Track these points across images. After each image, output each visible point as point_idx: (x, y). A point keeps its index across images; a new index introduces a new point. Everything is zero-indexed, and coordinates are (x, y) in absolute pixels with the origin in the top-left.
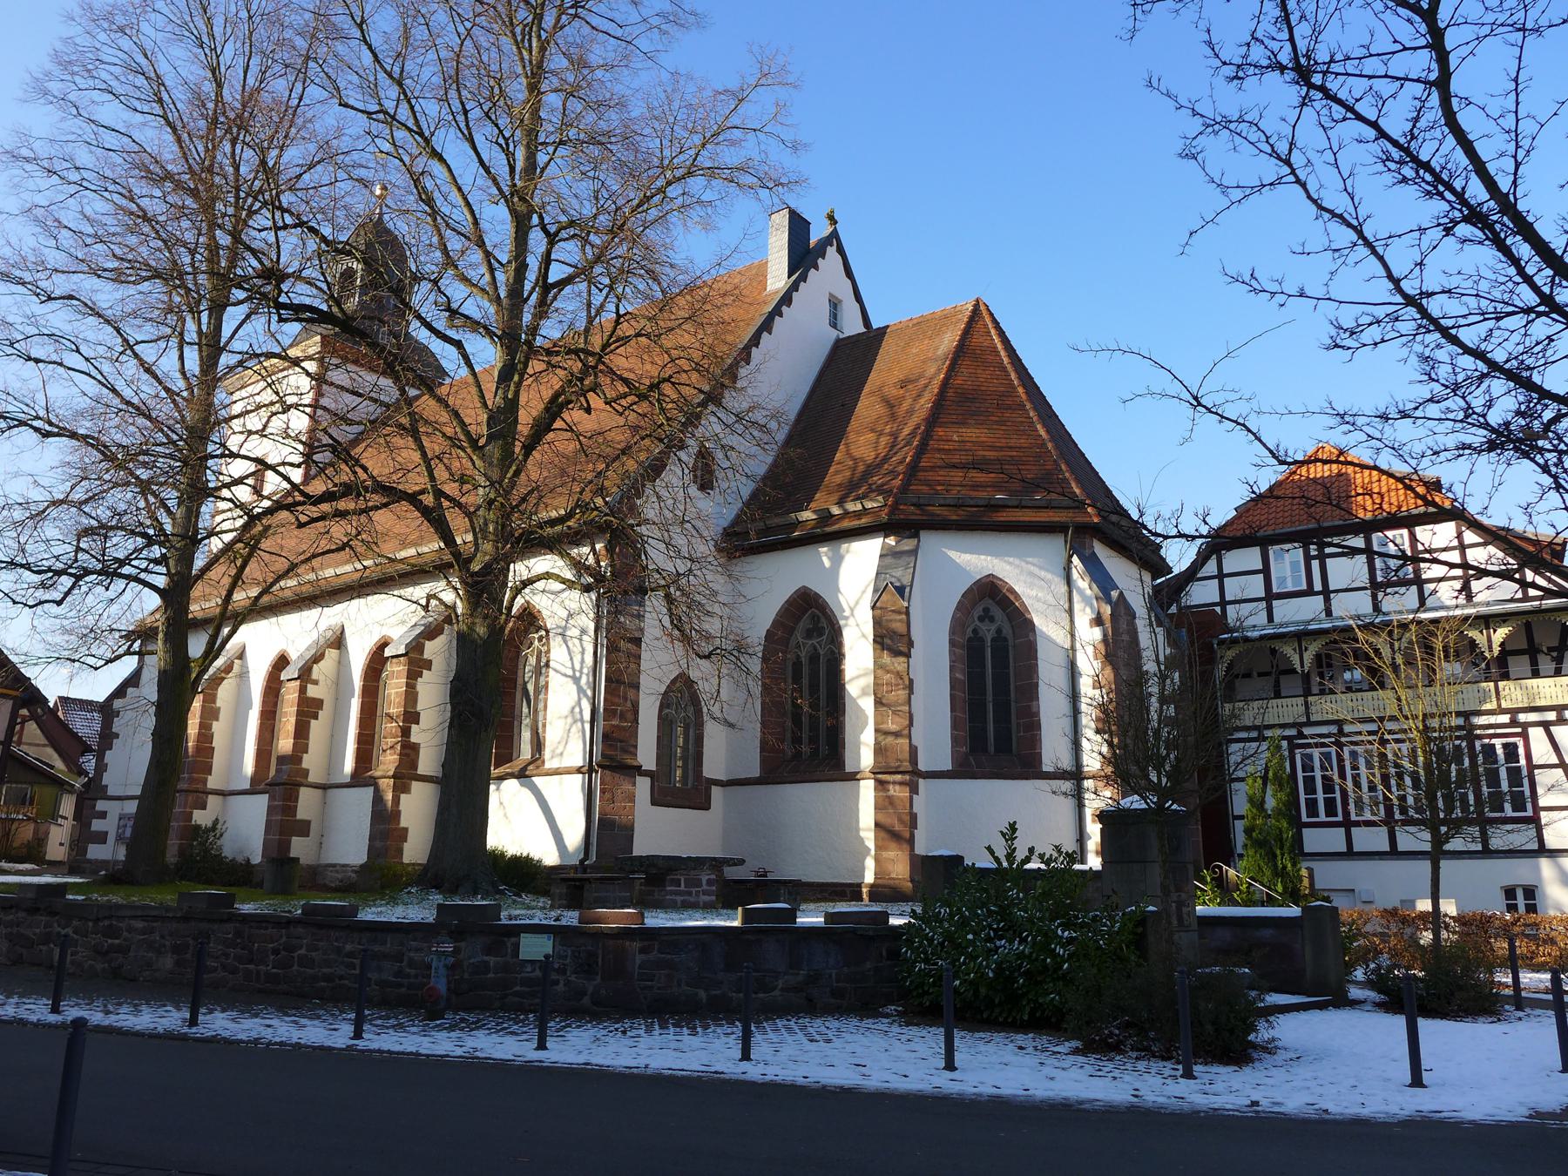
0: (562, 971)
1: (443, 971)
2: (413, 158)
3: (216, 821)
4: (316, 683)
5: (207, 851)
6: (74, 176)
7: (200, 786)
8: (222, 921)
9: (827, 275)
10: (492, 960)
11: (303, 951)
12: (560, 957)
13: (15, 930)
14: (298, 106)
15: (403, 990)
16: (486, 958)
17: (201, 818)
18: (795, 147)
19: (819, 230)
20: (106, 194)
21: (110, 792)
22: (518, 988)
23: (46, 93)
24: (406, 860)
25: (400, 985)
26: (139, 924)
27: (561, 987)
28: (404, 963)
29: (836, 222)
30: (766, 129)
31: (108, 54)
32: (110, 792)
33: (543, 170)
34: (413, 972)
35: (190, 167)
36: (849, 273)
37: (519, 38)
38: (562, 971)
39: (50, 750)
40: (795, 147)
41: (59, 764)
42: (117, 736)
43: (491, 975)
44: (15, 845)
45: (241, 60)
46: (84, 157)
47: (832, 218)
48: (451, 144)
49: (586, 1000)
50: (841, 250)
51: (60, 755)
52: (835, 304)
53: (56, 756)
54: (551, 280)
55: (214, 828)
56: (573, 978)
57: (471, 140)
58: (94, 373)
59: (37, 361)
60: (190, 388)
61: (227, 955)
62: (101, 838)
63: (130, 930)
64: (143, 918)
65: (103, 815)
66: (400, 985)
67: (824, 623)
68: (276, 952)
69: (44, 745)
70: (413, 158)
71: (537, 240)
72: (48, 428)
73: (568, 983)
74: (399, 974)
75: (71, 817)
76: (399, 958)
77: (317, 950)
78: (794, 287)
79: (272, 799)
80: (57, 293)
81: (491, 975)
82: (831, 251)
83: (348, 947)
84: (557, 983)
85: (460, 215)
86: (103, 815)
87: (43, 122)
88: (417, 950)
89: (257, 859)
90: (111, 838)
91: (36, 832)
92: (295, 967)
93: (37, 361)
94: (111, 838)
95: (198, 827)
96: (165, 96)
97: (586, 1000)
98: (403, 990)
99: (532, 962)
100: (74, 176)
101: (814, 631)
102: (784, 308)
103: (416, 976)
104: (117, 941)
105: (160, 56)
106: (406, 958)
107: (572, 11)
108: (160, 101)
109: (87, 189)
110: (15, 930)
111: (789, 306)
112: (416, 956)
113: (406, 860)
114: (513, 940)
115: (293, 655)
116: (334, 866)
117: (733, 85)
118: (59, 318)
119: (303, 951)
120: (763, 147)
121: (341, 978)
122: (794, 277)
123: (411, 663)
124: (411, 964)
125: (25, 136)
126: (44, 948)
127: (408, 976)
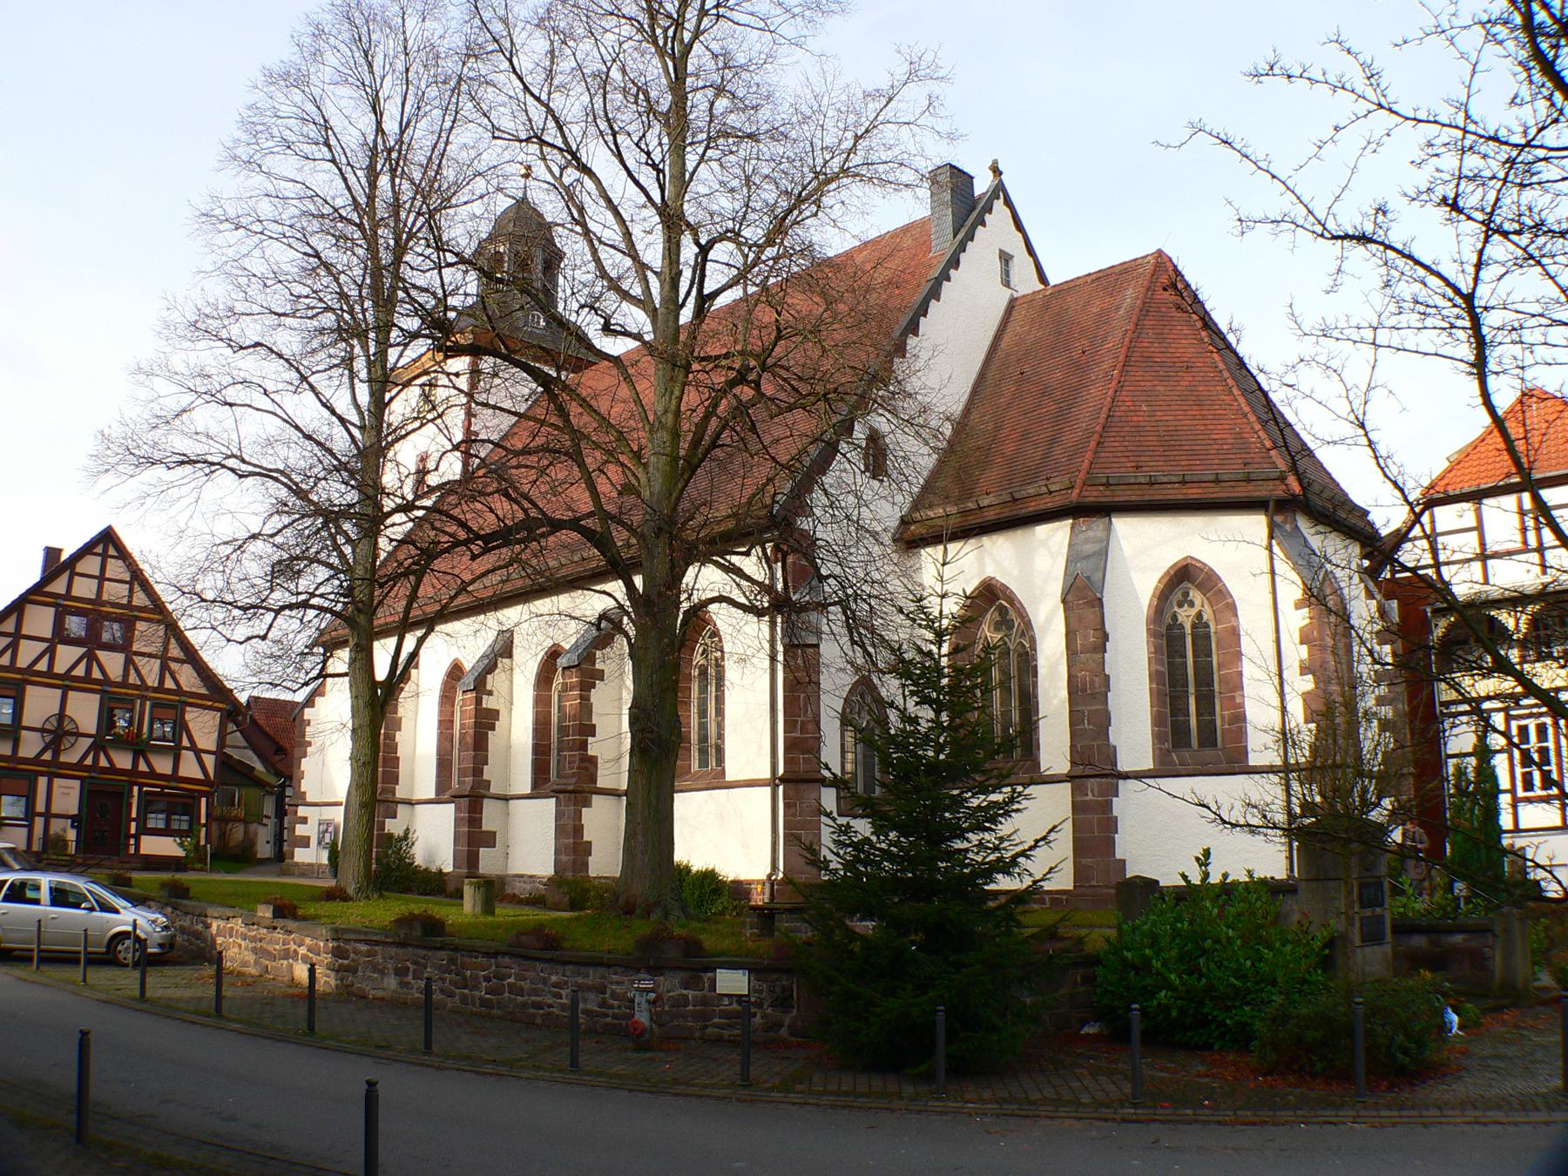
0: (760, 1005)
1: (644, 1005)
2: (562, 169)
3: (407, 831)
4: (490, 693)
5: (402, 859)
6: (257, 227)
7: (389, 796)
8: (436, 949)
9: (996, 231)
10: (690, 994)
11: (512, 980)
12: (756, 991)
13: (259, 945)
14: (452, 127)
15: (609, 1020)
16: (684, 992)
17: (394, 827)
18: (951, 137)
19: (982, 184)
20: (285, 240)
21: (309, 799)
22: (717, 1020)
23: (235, 158)
24: (592, 873)
25: (607, 1015)
26: (364, 948)
27: (757, 1020)
28: (607, 995)
29: (1001, 173)
30: (919, 122)
31: (285, 109)
32: (309, 799)
33: (692, 174)
34: (616, 1003)
35: (354, 199)
36: (1019, 226)
37: (661, 43)
38: (760, 1005)
39: (250, 753)
40: (951, 137)
41: (258, 766)
42: (310, 744)
43: (690, 1008)
44: (231, 844)
45: (398, 89)
46: (266, 208)
47: (996, 170)
48: (598, 157)
49: (784, 1032)
50: (1008, 203)
51: (259, 757)
52: (1005, 258)
53: (255, 758)
54: (706, 292)
55: (406, 837)
56: (769, 1011)
57: (619, 156)
58: (279, 412)
59: (231, 405)
60: (362, 418)
61: (443, 980)
62: (305, 842)
63: (356, 952)
64: (366, 942)
65: (304, 820)
66: (607, 1015)
67: (1012, 615)
68: (487, 979)
69: (245, 748)
70: (562, 169)
71: (688, 252)
72: (244, 467)
73: (764, 1016)
74: (603, 1004)
75: (273, 816)
76: (601, 990)
77: (525, 979)
78: (962, 248)
79: (457, 810)
80: (248, 343)
81: (690, 1008)
82: (999, 205)
83: (554, 978)
84: (755, 1015)
85: (612, 234)
86: (304, 820)
87: (236, 187)
88: (618, 983)
89: (448, 868)
90: (314, 842)
91: (246, 833)
92: (507, 994)
93: (231, 405)
94: (314, 842)
95: (391, 836)
96: (333, 141)
97: (784, 1032)
98: (609, 1020)
99: (730, 996)
100: (257, 227)
101: (1004, 623)
102: (952, 272)
103: (619, 1007)
104: (346, 962)
105: (327, 100)
106: (609, 991)
107: (714, 11)
108: (327, 144)
109: (271, 238)
110: (259, 945)
111: (957, 268)
112: (619, 989)
113: (592, 873)
114: (710, 974)
115: (468, 666)
116: (522, 876)
117: (884, 84)
118: (249, 364)
119: (512, 980)
120: (918, 138)
121: (550, 1006)
122: (960, 237)
123: (583, 673)
124: (614, 995)
125: (216, 198)
126: (285, 962)
127: (612, 1007)
